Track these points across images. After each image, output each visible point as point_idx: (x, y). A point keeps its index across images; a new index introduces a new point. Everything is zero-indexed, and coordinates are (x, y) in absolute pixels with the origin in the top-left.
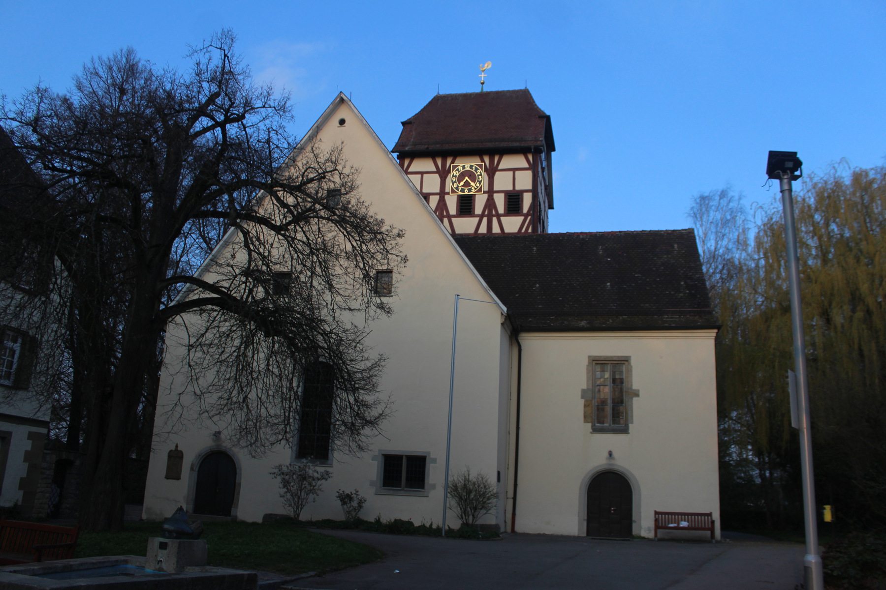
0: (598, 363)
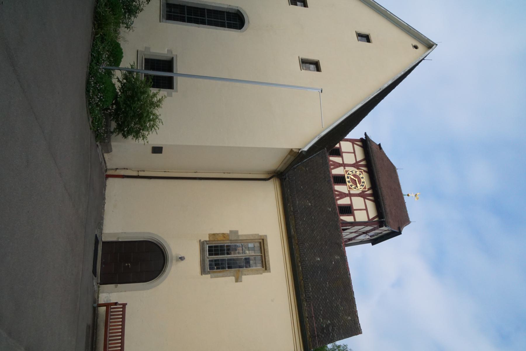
0: (262, 244)
